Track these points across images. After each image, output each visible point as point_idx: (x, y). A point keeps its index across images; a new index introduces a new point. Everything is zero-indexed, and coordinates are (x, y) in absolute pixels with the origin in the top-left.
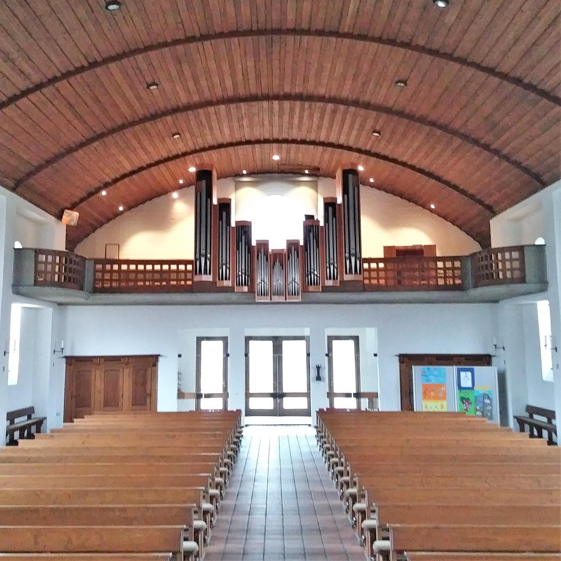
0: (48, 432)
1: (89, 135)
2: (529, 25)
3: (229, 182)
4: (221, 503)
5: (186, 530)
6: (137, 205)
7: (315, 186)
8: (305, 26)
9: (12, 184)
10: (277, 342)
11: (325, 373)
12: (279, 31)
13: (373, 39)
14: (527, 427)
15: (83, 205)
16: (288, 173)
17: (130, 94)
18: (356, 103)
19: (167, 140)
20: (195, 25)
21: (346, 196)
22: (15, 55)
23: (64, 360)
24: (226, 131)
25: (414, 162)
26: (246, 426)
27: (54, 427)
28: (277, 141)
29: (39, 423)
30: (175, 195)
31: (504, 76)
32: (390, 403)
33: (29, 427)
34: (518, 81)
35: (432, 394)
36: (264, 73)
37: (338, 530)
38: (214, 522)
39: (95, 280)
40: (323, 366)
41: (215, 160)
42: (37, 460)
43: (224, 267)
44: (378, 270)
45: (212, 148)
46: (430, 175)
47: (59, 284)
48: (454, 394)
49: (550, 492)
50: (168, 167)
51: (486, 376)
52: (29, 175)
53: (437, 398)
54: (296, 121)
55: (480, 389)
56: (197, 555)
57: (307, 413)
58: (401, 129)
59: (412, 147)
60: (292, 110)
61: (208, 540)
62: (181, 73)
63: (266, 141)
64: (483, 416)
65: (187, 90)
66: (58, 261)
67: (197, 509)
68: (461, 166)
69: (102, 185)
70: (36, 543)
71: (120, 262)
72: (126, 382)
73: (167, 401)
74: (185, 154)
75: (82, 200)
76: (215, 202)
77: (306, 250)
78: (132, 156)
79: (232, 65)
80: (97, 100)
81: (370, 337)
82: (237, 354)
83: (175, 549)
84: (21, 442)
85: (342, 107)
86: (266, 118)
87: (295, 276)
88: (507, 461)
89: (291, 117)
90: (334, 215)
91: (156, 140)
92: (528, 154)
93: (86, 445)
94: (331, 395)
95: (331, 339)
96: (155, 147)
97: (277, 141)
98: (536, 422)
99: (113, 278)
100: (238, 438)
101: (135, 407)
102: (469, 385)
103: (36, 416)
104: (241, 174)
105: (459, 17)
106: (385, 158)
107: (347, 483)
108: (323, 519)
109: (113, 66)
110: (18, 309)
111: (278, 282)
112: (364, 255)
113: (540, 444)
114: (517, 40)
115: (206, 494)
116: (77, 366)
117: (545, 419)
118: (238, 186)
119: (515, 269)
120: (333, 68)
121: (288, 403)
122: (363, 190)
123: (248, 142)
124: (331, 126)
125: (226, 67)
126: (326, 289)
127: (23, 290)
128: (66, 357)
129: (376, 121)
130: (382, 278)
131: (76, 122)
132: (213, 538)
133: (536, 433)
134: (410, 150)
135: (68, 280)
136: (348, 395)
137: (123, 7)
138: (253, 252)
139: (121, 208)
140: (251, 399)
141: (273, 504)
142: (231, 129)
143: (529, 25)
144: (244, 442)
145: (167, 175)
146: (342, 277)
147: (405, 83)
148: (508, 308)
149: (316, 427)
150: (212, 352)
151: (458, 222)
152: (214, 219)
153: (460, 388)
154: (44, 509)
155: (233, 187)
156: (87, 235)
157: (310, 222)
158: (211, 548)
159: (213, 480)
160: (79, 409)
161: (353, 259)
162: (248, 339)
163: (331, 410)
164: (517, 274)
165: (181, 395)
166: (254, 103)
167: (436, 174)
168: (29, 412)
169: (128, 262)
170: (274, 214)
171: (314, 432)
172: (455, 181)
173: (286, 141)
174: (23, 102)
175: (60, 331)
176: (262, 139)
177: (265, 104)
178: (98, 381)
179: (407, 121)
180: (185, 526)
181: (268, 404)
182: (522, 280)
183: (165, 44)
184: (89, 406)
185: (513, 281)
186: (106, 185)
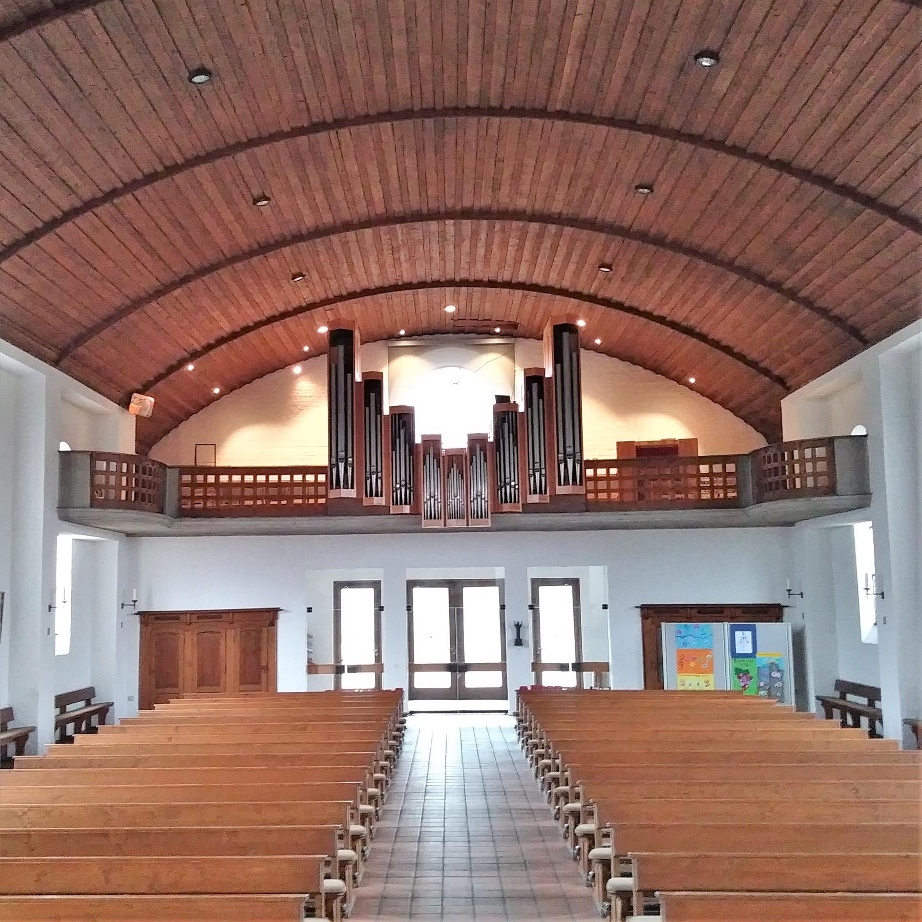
0: (117, 723)
1: (166, 277)
2: (845, 92)
3: (379, 348)
4: (376, 825)
7: (510, 351)
9: (53, 354)
10: (455, 589)
12: (455, 111)
14: (836, 712)
15: (160, 385)
16: (469, 333)
17: (228, 216)
18: (574, 222)
19: (284, 282)
21: (559, 366)
22: (52, 157)
24: (374, 270)
25: (664, 311)
28: (451, 283)
29: (103, 712)
30: (297, 369)
31: (806, 175)
32: (627, 676)
33: (87, 716)
34: (826, 182)
35: (692, 664)
36: (432, 177)
37: (552, 864)
39: (181, 497)
43: (374, 477)
44: (608, 478)
45: (352, 295)
47: (127, 505)
49: (874, 805)
50: (285, 326)
51: (774, 639)
52: (79, 340)
53: (699, 671)
54: (481, 251)
55: (763, 658)
56: (344, 901)
57: (501, 694)
58: (644, 261)
59: (660, 288)
60: (475, 234)
62: (304, 179)
63: (436, 284)
64: (770, 696)
70: (107, 881)
71: (218, 471)
73: (291, 676)
74: (312, 306)
76: (358, 378)
77: (498, 449)
78: (232, 310)
79: (382, 167)
81: (595, 580)
82: (393, 610)
86: (435, 247)
87: (482, 489)
88: (806, 760)
90: (541, 395)
92: (843, 296)
93: (174, 742)
94: (538, 667)
95: (537, 583)
96: (266, 295)
97: (451, 283)
100: (399, 730)
101: (243, 687)
104: (396, 335)
105: (734, 84)
106: (619, 306)
107: (565, 795)
109: (201, 171)
110: (66, 543)
111: (456, 499)
112: (588, 456)
116: (158, 628)
117: (864, 701)
118: (393, 354)
119: (820, 474)
120: (537, 170)
121: (472, 680)
122: (587, 359)
123: (408, 286)
125: (373, 171)
126: (529, 509)
127: (73, 513)
128: (139, 613)
129: (606, 248)
136: (563, 667)
140: (417, 675)
141: (454, 824)
142: (382, 266)
143: (845, 92)
144: (408, 737)
145: (285, 338)
146: (553, 489)
147: (650, 187)
148: (809, 533)
150: (358, 605)
152: (357, 405)
153: (734, 655)
155: (385, 353)
157: (504, 407)
158: (363, 891)
160: (161, 690)
161: (570, 462)
162: (411, 584)
164: (823, 481)
165: (312, 668)
166: (418, 225)
168: (87, 695)
171: (513, 721)
173: (465, 283)
174: (67, 229)
175: (130, 573)
176: (429, 280)
177: (434, 225)
178: (188, 648)
181: (444, 680)
182: (831, 490)
184: (176, 686)
185: (817, 491)
186: (194, 356)
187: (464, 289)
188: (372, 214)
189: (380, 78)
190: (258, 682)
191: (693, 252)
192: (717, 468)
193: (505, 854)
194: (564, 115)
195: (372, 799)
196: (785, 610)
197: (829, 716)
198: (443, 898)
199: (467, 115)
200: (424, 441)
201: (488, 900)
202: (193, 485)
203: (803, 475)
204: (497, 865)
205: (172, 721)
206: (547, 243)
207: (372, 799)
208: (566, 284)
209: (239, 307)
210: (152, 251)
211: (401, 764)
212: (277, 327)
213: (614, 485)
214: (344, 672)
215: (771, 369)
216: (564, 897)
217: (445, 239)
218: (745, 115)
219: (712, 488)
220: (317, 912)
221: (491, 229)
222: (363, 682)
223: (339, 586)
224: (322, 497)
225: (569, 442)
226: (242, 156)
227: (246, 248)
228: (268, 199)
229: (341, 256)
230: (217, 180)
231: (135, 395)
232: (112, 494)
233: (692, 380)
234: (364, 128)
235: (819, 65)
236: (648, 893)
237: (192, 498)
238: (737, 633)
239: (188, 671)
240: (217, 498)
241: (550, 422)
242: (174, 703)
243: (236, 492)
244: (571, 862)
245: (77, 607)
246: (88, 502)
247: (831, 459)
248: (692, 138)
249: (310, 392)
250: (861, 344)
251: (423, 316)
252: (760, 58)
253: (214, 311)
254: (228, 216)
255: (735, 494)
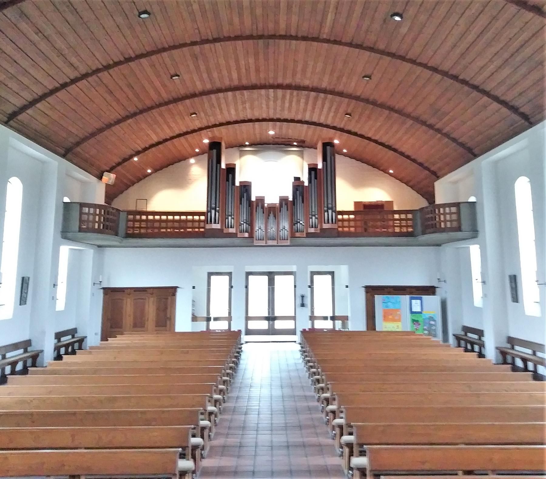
0: (88, 348)
1: (123, 113)
2: (463, 36)
3: (235, 150)
4: (224, 405)
5: (194, 428)
6: (161, 169)
7: (301, 155)
8: (293, 33)
9: (62, 151)
10: (271, 276)
11: (308, 301)
12: (273, 37)
13: (346, 44)
14: (463, 343)
15: (119, 168)
16: (281, 144)
17: (158, 84)
18: (332, 92)
19: (186, 118)
20: (208, 31)
22: (66, 52)
23: (102, 290)
24: (233, 112)
25: (376, 138)
26: (247, 342)
27: (93, 344)
29: (81, 341)
30: (192, 161)
31: (445, 74)
32: (357, 324)
33: (72, 344)
34: (455, 78)
35: (390, 317)
36: (262, 68)
37: (314, 427)
38: (217, 421)
39: (128, 227)
40: (306, 295)
41: (224, 134)
42: (76, 372)
44: (349, 220)
45: (221, 124)
46: (389, 147)
47: (99, 231)
48: (407, 318)
49: (478, 396)
50: (187, 140)
51: (431, 304)
52: (78, 144)
53: (394, 320)
54: (287, 105)
55: (427, 313)
56: (203, 449)
57: (292, 332)
58: (367, 112)
59: (374, 125)
60: (284, 97)
61: (212, 435)
62: (197, 68)
64: (430, 334)
65: (202, 80)
66: (98, 213)
67: (203, 411)
68: (412, 141)
69: (134, 153)
70: (73, 440)
71: (148, 213)
72: (151, 309)
73: (183, 323)
74: (201, 129)
75: (119, 164)
76: (223, 166)
77: (294, 205)
78: (158, 130)
79: (237, 61)
80: (130, 86)
81: (343, 272)
82: (239, 286)
83: (184, 445)
84: (65, 357)
85: (322, 95)
86: (264, 102)
87: (285, 224)
88: (445, 370)
89: (283, 102)
90: (316, 178)
91: (177, 117)
92: (464, 133)
93: (117, 360)
94: (312, 318)
95: (313, 273)
96: (177, 123)
98: (469, 339)
99: (142, 226)
100: (238, 353)
101: (157, 328)
102: (419, 310)
103: (79, 335)
105: (410, 29)
106: (355, 134)
107: (322, 389)
108: (304, 417)
109: (143, 61)
110: (65, 250)
111: (272, 230)
113: (472, 357)
114: (455, 46)
115: (210, 399)
117: (476, 337)
118: (242, 154)
119: (454, 220)
120: (314, 67)
121: (279, 325)
122: (339, 159)
123: (250, 121)
124: (314, 108)
125: (232, 63)
126: (309, 235)
127: (69, 235)
128: (104, 288)
129: (348, 105)
130: (352, 227)
131: (114, 104)
132: (217, 434)
133: (469, 347)
134: (374, 129)
135: (106, 227)
136: (325, 318)
137: (152, 16)
138: (253, 205)
139: (149, 171)
140: (249, 322)
141: (265, 405)
142: (236, 110)
143: (463, 36)
144: (243, 356)
145: (186, 145)
146: (321, 226)
147: (369, 77)
148: (448, 250)
149: (300, 344)
150: (220, 284)
151: (411, 184)
152: (222, 180)
153: (412, 312)
154: (80, 413)
156: (122, 192)
157: (297, 183)
158: (215, 442)
159: (217, 387)
160: (113, 330)
162: (248, 274)
163: (313, 330)
164: (455, 224)
165: (194, 318)
166: (255, 91)
167: (393, 147)
168: (73, 332)
169: (154, 213)
170: (270, 176)
171: (299, 347)
172: (408, 153)
173: (279, 120)
174: (73, 88)
175: (99, 267)
177: (263, 92)
178: (128, 307)
179: (372, 106)
180: (193, 426)
181: (264, 325)
183: (184, 45)
184: (121, 327)
185: (452, 230)
186: (138, 153)
187: (278, 123)
188: (232, 85)
189: (236, 20)
190: (165, 326)
191: (391, 109)
192: (403, 216)
193: (290, 421)
194: (327, 41)
195: (221, 392)
196: (437, 289)
197: (459, 346)
198: (256, 447)
199: (280, 39)
200: (256, 200)
201: (280, 447)
202: (134, 221)
203: (445, 221)
204: (286, 427)
205: (117, 348)
206: (319, 103)
207: (221, 392)
208: (329, 122)
209: (162, 130)
210: (118, 101)
211: (239, 371)
212: (182, 139)
213: (352, 224)
214: (210, 320)
215: (430, 167)
216: (320, 445)
217: (269, 98)
218: (416, 44)
219: (401, 227)
220: (186, 457)
221: (291, 94)
222: (223, 326)
223: (210, 274)
224: (202, 228)
225: (330, 201)
226: (165, 54)
227: (166, 100)
228: (178, 76)
229: (216, 105)
230: (153, 66)
231: (105, 173)
232: (90, 225)
233: (391, 171)
234: (228, 43)
235: (452, 21)
236: (361, 445)
237: (133, 228)
238: (413, 301)
239: (128, 319)
240: (147, 228)
241: (321, 189)
242: (119, 337)
243: (157, 225)
244: (325, 425)
245: (76, 282)
246: (77, 229)
247: (458, 213)
248: (389, 54)
249: (198, 173)
250: (472, 156)
251: (258, 136)
252: (422, 18)
253: (149, 130)
254: (158, 84)
255: (411, 230)
